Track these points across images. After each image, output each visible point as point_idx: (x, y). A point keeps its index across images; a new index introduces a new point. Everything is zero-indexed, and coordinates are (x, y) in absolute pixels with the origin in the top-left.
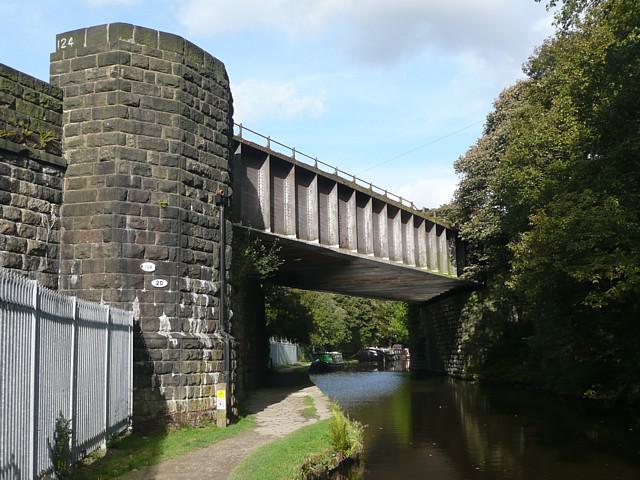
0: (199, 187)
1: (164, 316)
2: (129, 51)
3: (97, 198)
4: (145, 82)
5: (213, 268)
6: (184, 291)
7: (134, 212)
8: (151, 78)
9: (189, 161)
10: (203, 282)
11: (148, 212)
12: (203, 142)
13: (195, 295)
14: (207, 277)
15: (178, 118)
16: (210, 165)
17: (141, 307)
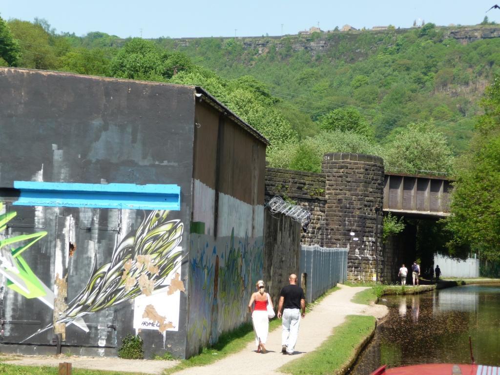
0: (369, 206)
8: (354, 172)
10: (370, 238)
11: (353, 216)
13: (367, 243)
14: (371, 236)
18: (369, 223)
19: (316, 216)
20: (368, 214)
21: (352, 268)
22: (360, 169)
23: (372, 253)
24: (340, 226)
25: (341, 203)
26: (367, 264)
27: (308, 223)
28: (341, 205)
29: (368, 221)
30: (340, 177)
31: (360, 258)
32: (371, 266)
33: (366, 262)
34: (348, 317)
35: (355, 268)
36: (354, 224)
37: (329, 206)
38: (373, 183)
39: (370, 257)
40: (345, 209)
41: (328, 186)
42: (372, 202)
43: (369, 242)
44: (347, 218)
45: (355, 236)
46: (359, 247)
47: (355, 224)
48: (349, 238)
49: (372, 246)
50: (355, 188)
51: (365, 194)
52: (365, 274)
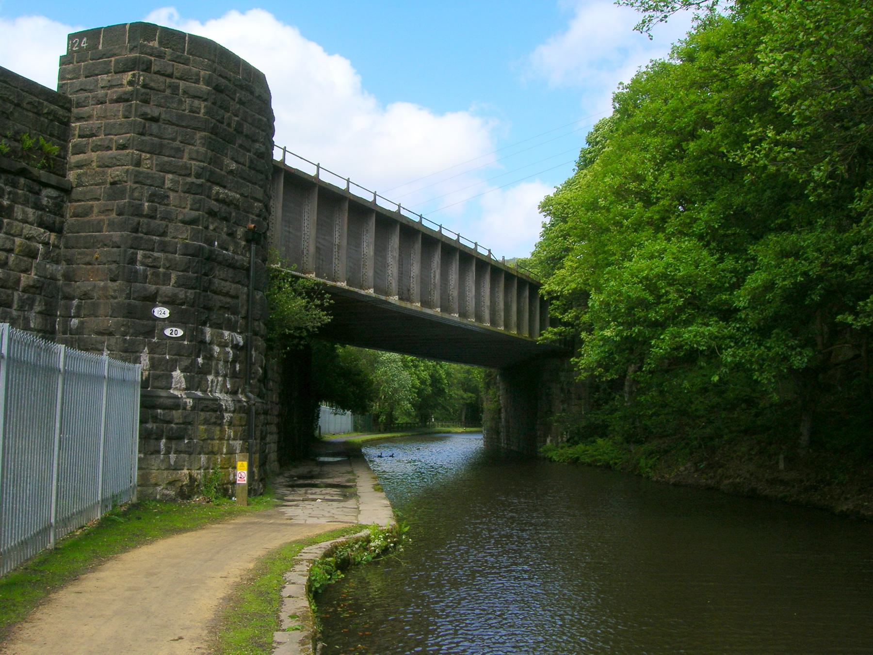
0: (226, 219)
1: (178, 371)
2: (151, 55)
7: (146, 247)
8: (175, 88)
10: (226, 333)
11: (163, 248)
13: (217, 349)
18: (222, 280)
19: (18, 240)
20: (223, 247)
21: (159, 439)
22: (197, 82)
23: (233, 385)
24: (113, 280)
26: (215, 423)
29: (220, 272)
31: (190, 402)
33: (212, 416)
34: (546, 206)
35: (169, 439)
36: (166, 279)
37: (80, 210)
38: (241, 146)
39: (225, 400)
40: (136, 219)
41: (76, 140)
42: (237, 207)
43: (223, 345)
45: (171, 321)
48: (152, 327)
49: (234, 361)
51: (212, 172)
52: (209, 459)
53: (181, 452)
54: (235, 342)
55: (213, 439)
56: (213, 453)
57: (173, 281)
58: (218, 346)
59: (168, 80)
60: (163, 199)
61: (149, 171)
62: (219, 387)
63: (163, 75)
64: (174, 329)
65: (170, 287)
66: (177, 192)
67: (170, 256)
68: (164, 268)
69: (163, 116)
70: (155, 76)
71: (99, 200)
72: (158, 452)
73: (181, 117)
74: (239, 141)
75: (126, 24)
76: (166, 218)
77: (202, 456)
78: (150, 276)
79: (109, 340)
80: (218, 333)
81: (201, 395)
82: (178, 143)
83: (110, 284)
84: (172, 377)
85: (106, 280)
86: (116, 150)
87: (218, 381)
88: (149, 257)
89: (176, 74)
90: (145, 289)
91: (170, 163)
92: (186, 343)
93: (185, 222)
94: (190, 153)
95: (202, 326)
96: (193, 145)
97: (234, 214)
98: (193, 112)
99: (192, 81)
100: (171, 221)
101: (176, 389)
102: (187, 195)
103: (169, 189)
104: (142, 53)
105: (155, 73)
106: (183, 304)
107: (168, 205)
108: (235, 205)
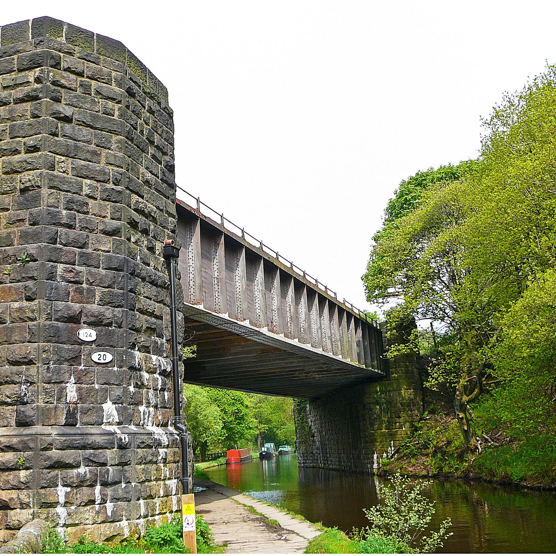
0: (145, 232)
1: (109, 403)
2: (59, 51)
3: (16, 242)
4: (79, 91)
5: (164, 341)
6: (132, 368)
7: (67, 259)
8: (86, 88)
9: (135, 197)
10: (154, 357)
11: (86, 260)
12: (149, 176)
13: (146, 375)
14: (158, 351)
15: (119, 142)
16: (158, 208)
17: (79, 390)
21: (92, 486)
24: (29, 299)
25: (36, 200)
26: (151, 462)
27: (34, 383)
28: (35, 210)
30: (31, 98)
32: (166, 471)
40: (54, 228)
44: (60, 267)
46: (118, 392)
47: (98, 292)
49: (163, 390)
50: (93, 147)
52: (147, 505)
53: (118, 500)
54: (163, 368)
55: (150, 481)
56: (151, 497)
57: (97, 298)
58: (147, 372)
59: (80, 79)
60: (82, 207)
61: (65, 175)
62: (150, 419)
63: (73, 72)
64: (102, 353)
65: (95, 306)
66: (96, 199)
67: (93, 270)
68: (87, 284)
69: (76, 116)
70: (65, 74)
71: (8, 210)
72: (93, 502)
73: (95, 117)
74: (151, 150)
75: (29, 20)
76: (87, 228)
77: (142, 501)
78: (72, 294)
79: (28, 370)
80: (146, 357)
81: (135, 429)
82: (93, 146)
83: (26, 303)
84: (103, 411)
85: (21, 299)
86: (26, 153)
87: (149, 412)
88: (71, 271)
89: (87, 73)
90: (69, 308)
91: (87, 167)
92: (115, 369)
93: (105, 233)
94: (107, 158)
95: (132, 349)
96: (109, 149)
97: (152, 227)
98: (108, 114)
99: (104, 81)
100: (92, 231)
101: (110, 424)
102: (107, 203)
103: (87, 195)
104: (50, 48)
105: (65, 70)
106: (110, 324)
107: (87, 213)
108: (153, 217)
